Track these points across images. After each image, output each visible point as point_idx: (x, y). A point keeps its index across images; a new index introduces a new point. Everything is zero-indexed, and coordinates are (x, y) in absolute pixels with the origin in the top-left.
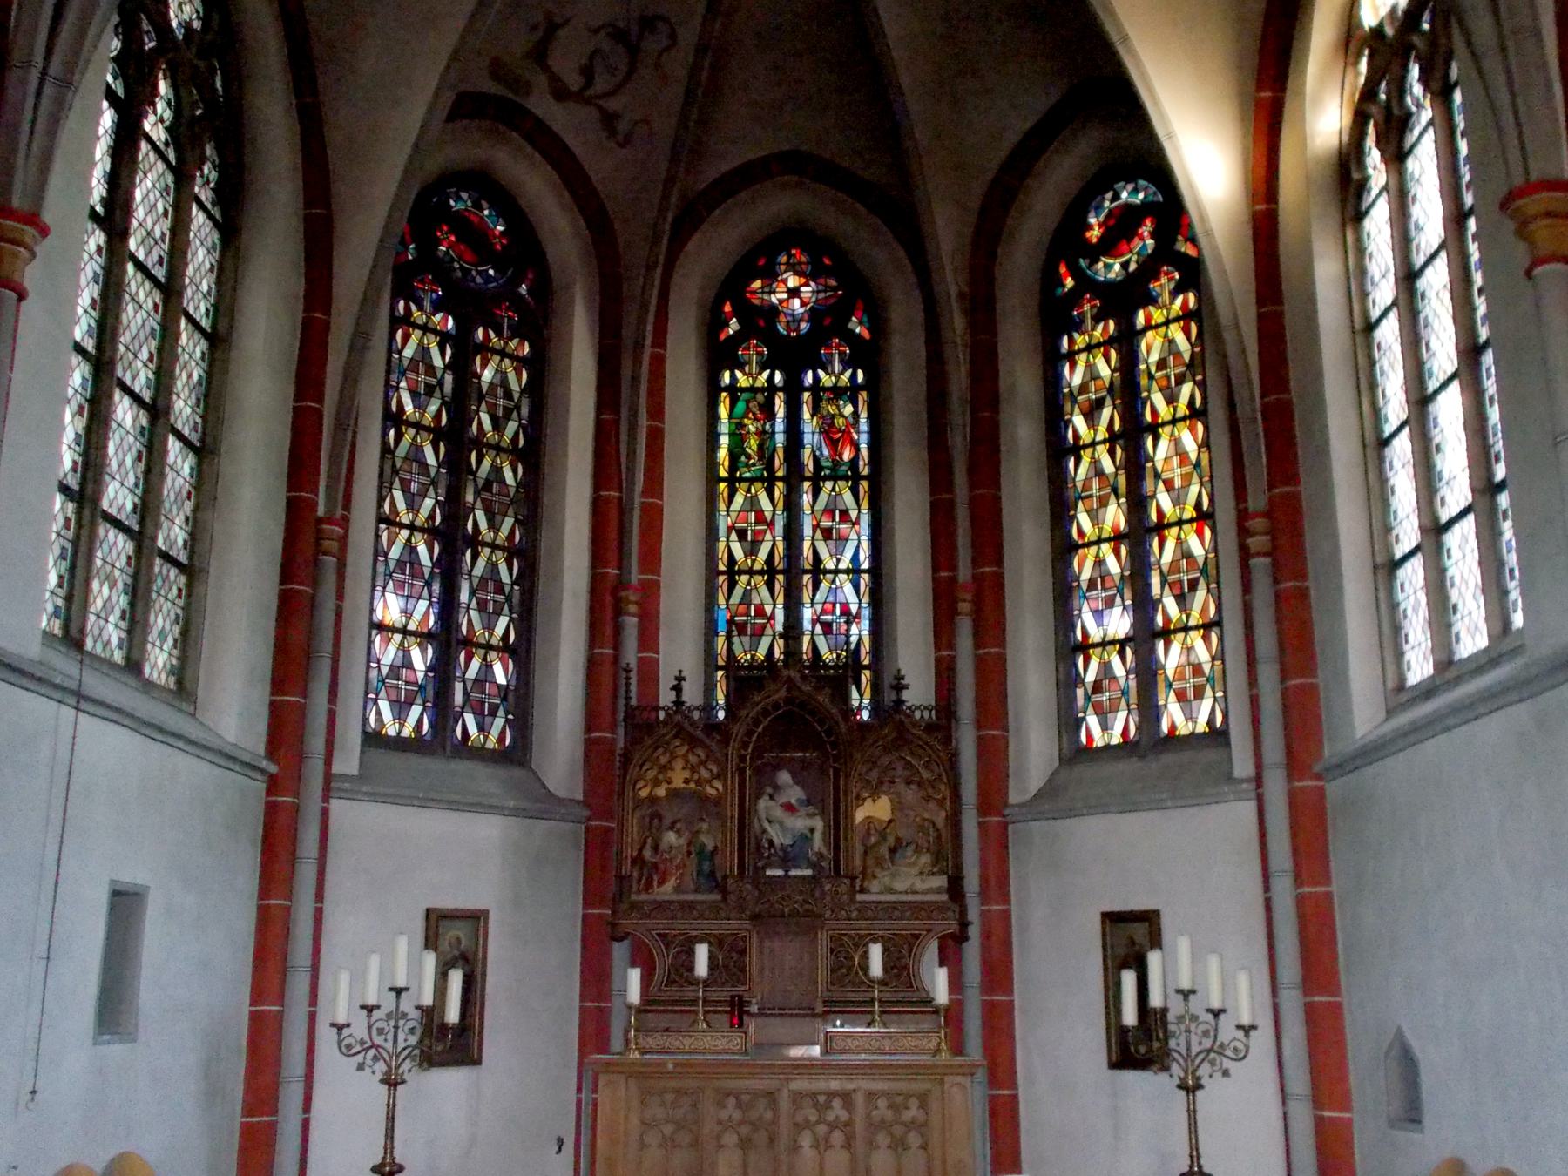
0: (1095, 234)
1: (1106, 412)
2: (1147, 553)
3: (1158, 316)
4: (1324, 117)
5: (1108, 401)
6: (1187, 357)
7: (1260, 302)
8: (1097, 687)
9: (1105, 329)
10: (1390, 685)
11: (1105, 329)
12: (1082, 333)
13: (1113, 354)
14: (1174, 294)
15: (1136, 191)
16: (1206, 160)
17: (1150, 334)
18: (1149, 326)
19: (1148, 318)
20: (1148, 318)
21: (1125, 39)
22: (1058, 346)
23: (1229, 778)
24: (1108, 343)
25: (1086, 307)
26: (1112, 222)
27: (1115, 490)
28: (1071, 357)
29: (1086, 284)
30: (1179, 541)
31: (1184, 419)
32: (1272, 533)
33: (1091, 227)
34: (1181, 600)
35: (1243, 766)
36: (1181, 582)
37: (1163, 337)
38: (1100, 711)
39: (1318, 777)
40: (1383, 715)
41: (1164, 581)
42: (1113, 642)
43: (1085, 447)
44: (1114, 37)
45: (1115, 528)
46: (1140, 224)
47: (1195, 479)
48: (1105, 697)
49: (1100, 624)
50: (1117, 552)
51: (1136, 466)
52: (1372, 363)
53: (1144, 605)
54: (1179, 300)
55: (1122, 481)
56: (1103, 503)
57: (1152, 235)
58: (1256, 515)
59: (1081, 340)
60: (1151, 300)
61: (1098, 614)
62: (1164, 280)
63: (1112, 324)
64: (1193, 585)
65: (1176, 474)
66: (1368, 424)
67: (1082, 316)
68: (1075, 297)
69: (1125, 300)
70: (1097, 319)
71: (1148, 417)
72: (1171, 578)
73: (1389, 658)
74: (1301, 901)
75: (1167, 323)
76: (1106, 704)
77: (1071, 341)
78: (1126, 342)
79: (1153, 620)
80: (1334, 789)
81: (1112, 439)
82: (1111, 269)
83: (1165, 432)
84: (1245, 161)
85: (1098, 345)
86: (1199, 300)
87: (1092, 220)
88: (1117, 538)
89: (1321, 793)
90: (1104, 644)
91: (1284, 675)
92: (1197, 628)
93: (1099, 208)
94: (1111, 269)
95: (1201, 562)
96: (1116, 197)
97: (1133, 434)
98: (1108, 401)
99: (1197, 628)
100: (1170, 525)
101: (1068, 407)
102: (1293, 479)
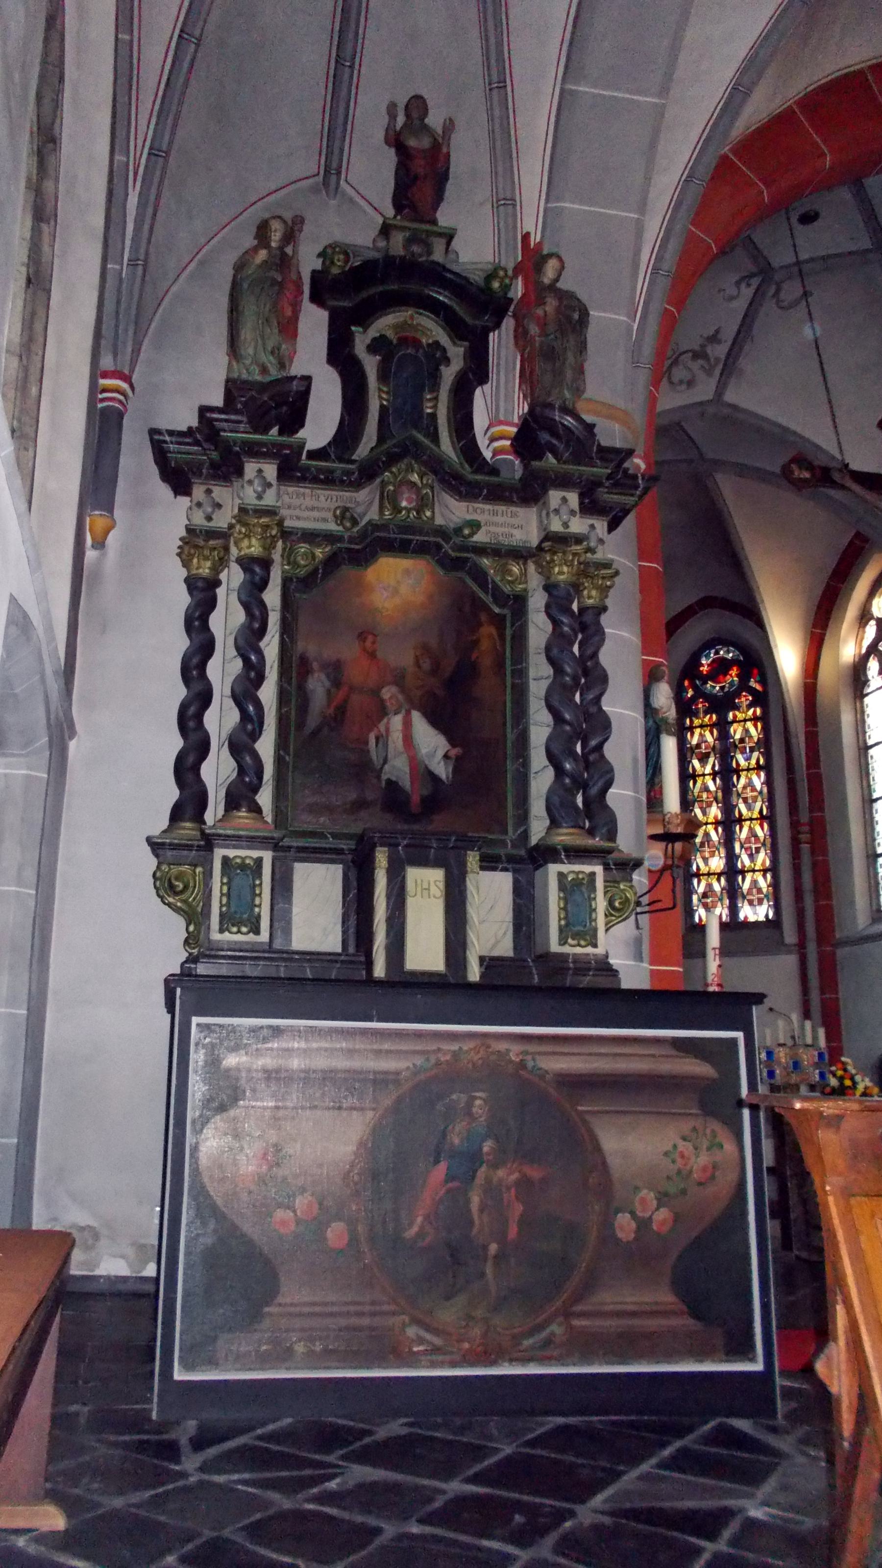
0: (704, 669)
1: (711, 760)
2: (734, 832)
3: (740, 716)
4: (847, 647)
5: (712, 755)
6: (756, 739)
7: (807, 726)
8: (705, 895)
9: (711, 718)
10: (874, 908)
11: (711, 718)
12: (697, 718)
13: (715, 732)
14: (749, 707)
15: (728, 652)
16: (788, 657)
17: (735, 725)
18: (735, 721)
19: (735, 716)
20: (735, 716)
21: (763, 601)
22: (685, 723)
23: (781, 942)
24: (712, 726)
25: (700, 706)
26: (715, 665)
27: (716, 799)
28: (691, 729)
29: (700, 693)
30: (750, 829)
31: (753, 769)
32: (812, 832)
33: (703, 665)
34: (751, 857)
35: (790, 936)
36: (751, 848)
37: (745, 727)
38: (706, 906)
39: (832, 945)
40: (870, 921)
41: (742, 847)
42: (714, 874)
43: (699, 776)
44: (759, 601)
45: (716, 817)
46: (730, 669)
47: (759, 799)
48: (709, 900)
49: (706, 864)
50: (716, 830)
51: (727, 789)
52: (867, 764)
53: (731, 858)
54: (752, 710)
55: (720, 794)
56: (709, 805)
57: (737, 676)
58: (804, 825)
59: (697, 722)
60: (737, 708)
61: (706, 860)
62: (743, 699)
63: (714, 717)
64: (758, 850)
65: (749, 794)
66: (866, 792)
67: (697, 709)
68: (694, 699)
69: (722, 705)
70: (706, 713)
71: (734, 765)
72: (746, 845)
73: (874, 896)
74: (823, 1001)
75: (745, 720)
76: (710, 905)
77: (692, 722)
78: (722, 727)
79: (772, 877)
80: (842, 953)
81: (714, 775)
82: (713, 687)
83: (743, 774)
84: (803, 658)
85: (707, 726)
86: (763, 712)
87: (704, 662)
88: (717, 823)
89: (834, 954)
90: (709, 874)
91: (816, 901)
92: (759, 871)
93: (708, 656)
94: (713, 687)
95: (762, 839)
96: (717, 653)
97: (727, 773)
98: (712, 755)
99: (759, 871)
100: (745, 820)
101: (689, 755)
102: (821, 809)
